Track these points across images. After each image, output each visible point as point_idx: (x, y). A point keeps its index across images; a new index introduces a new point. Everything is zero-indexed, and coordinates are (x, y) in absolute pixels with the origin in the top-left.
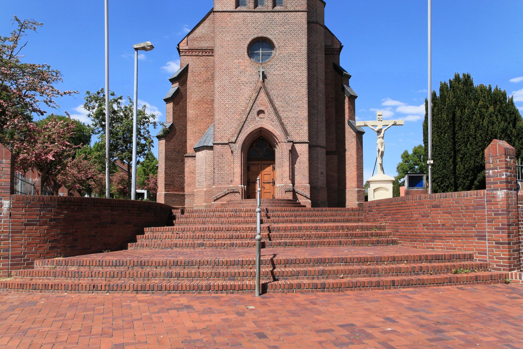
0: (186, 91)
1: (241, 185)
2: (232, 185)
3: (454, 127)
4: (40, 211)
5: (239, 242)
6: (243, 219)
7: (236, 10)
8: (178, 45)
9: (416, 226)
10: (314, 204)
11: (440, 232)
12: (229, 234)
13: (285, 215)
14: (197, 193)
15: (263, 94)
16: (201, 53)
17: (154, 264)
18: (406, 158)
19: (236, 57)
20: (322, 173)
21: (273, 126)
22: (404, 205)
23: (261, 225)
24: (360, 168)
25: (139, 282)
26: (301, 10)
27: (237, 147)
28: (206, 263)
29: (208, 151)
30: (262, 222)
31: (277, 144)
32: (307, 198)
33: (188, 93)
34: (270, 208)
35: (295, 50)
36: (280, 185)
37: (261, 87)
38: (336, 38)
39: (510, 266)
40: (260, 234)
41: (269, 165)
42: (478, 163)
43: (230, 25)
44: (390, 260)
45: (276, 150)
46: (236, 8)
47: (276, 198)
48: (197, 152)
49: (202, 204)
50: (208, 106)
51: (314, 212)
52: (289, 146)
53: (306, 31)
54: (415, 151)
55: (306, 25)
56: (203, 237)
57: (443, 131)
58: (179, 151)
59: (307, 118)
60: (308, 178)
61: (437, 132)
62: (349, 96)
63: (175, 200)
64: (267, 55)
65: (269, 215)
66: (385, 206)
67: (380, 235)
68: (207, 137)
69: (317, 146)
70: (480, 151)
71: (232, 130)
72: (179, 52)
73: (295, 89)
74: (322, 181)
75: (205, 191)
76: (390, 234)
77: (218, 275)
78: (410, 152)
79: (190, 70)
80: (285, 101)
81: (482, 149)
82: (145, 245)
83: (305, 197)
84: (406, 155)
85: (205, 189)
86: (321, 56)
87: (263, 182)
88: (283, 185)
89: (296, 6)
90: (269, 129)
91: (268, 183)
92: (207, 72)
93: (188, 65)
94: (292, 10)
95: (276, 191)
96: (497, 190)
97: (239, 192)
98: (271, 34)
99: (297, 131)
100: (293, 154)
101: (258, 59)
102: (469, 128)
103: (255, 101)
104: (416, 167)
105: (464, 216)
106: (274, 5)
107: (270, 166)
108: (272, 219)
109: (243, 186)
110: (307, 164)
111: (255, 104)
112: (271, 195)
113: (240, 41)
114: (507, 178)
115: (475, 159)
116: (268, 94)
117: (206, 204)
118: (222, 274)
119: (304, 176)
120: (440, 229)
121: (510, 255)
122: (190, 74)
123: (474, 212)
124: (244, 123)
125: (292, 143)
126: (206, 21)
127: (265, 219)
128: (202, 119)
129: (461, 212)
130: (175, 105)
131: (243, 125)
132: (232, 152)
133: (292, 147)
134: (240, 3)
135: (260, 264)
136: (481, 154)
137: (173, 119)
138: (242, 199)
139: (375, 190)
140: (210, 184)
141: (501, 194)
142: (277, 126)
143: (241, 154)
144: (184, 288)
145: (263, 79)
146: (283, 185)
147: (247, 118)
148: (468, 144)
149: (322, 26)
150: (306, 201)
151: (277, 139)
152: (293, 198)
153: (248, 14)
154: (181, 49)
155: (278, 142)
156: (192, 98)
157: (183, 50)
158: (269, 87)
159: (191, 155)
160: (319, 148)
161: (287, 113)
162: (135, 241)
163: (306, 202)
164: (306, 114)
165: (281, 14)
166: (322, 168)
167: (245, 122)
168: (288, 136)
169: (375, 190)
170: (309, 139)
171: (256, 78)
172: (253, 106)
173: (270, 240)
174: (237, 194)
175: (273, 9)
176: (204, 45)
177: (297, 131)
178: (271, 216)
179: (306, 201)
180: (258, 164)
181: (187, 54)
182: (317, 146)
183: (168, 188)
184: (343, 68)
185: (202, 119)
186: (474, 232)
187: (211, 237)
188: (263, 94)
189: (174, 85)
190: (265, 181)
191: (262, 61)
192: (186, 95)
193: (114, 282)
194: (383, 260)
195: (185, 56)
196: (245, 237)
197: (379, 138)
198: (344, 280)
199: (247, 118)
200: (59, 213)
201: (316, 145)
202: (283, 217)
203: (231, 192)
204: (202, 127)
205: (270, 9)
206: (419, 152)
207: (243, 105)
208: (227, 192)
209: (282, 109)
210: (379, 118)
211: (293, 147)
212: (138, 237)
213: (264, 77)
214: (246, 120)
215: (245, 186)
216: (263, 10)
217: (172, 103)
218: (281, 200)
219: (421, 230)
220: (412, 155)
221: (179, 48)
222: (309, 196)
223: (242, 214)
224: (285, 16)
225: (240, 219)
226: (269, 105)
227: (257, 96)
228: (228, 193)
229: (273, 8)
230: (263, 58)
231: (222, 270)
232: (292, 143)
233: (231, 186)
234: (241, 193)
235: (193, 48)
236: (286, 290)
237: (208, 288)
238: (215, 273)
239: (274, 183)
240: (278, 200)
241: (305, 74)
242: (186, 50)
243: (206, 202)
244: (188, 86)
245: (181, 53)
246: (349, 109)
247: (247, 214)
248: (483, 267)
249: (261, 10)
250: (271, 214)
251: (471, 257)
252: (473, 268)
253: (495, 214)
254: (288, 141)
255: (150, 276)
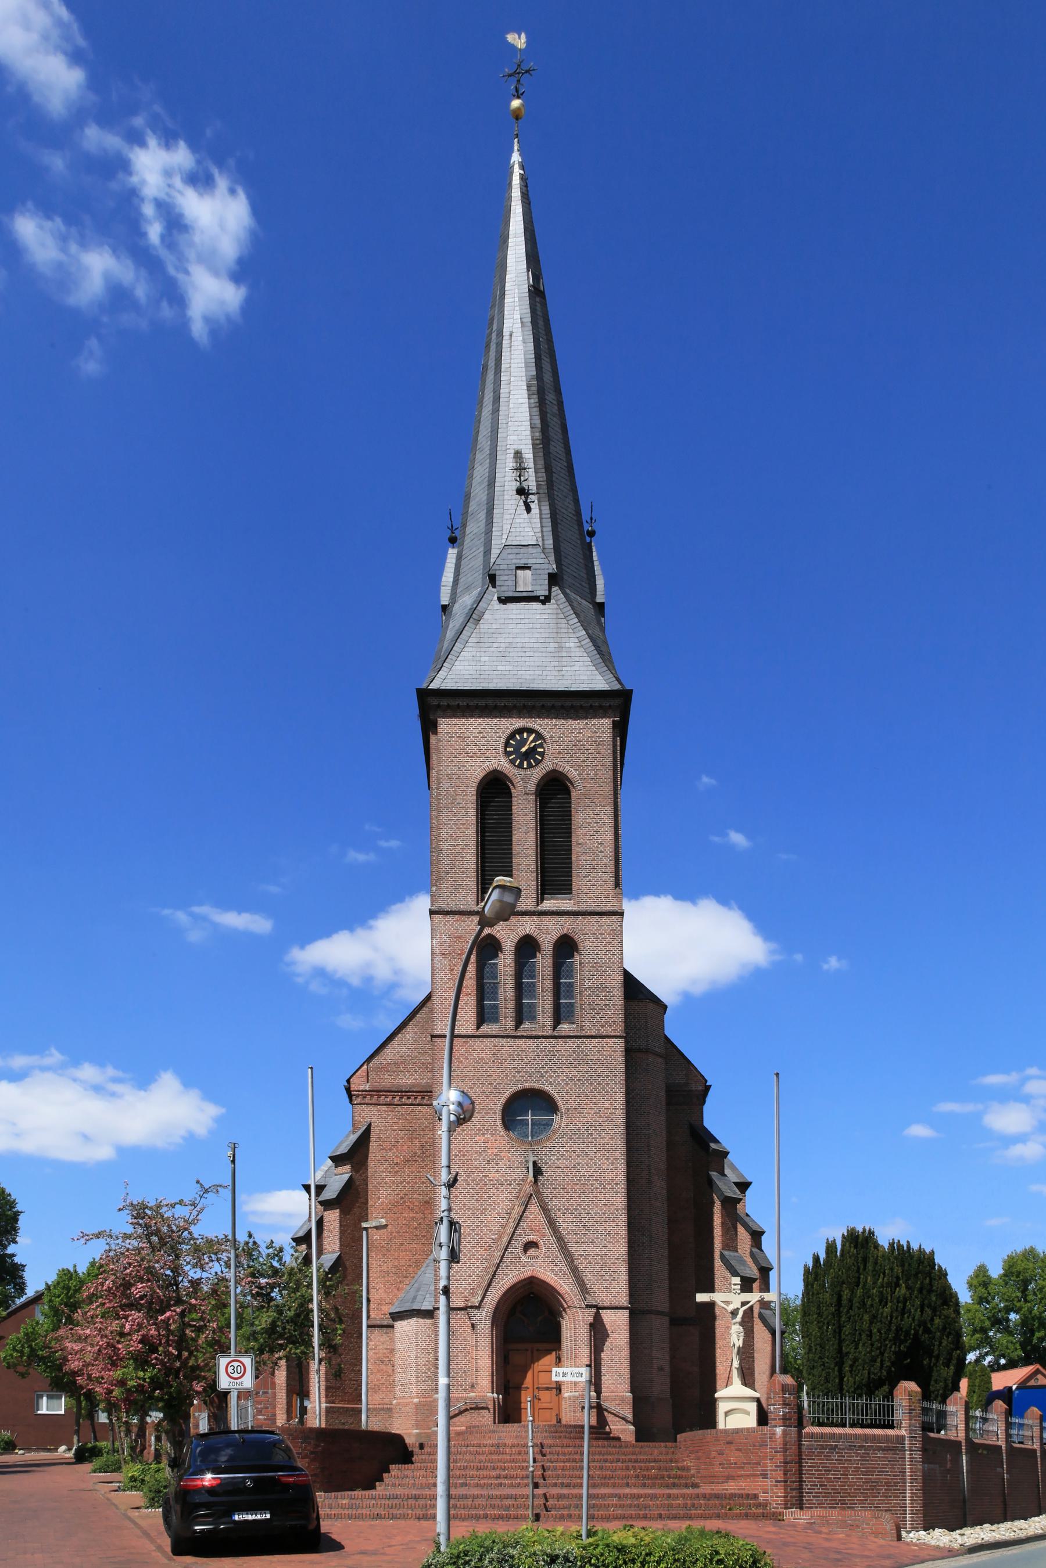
0: (365, 1181)
1: (493, 1393)
2: (474, 1394)
3: (840, 1317)
4: (302, 1443)
5: (506, 1481)
6: (508, 1457)
7: (477, 1033)
8: (348, 1081)
9: (713, 1465)
10: (643, 1434)
11: (732, 1472)
12: (494, 1473)
13: (566, 1452)
14: (398, 1407)
15: (534, 1209)
16: (398, 1098)
17: (428, 1497)
18: (982, 1290)
19: (479, 1130)
20: (661, 1369)
21: (556, 1274)
22: (704, 1441)
23: (535, 1490)
24: (747, 1357)
25: (419, 1512)
26: (613, 1034)
27: (484, 1317)
28: (480, 1497)
29: (421, 1320)
30: (535, 1461)
31: (564, 1310)
32: (627, 1422)
33: (370, 1187)
34: (545, 1442)
35: (600, 1117)
36: (572, 1394)
37: (531, 1195)
38: (696, 1069)
39: (785, 1504)
40: (533, 1467)
41: (548, 1352)
42: (874, 1374)
43: (465, 1063)
44: (665, 1496)
45: (563, 1323)
46: (478, 1027)
47: (564, 1422)
48: (397, 1321)
49: (409, 1431)
50: (414, 1215)
51: (610, 1449)
52: (589, 1316)
53: (623, 1078)
54: (1011, 1267)
55: (623, 1066)
56: (464, 1476)
57: (826, 1322)
58: (353, 1315)
59: (625, 1257)
60: (628, 1382)
61: (818, 1322)
62: (722, 1198)
63: (347, 1422)
64: (544, 1125)
65: (544, 1452)
66: (690, 1442)
67: (680, 1477)
68: (418, 1290)
69: (650, 1312)
70: (878, 1356)
71: (473, 1281)
72: (351, 1100)
73: (601, 1197)
74: (660, 1386)
75: (416, 1405)
76: (693, 1476)
77: (493, 1507)
78: (996, 1271)
79: (373, 1136)
80: (581, 1221)
81: (880, 1352)
82: (397, 1484)
83: (624, 1419)
84: (981, 1279)
85: (416, 1400)
86: (657, 1121)
87: (535, 1387)
88: (577, 1394)
89: (602, 1026)
90: (548, 1280)
91: (547, 1389)
92: (411, 1139)
93: (370, 1125)
94: (594, 1034)
95: (564, 1406)
96: (776, 1426)
97: (487, 1408)
98: (551, 1083)
99: (605, 1284)
100: (598, 1333)
101: (524, 1133)
102: (861, 1320)
103: (518, 1223)
104: (1013, 1316)
105: (752, 1453)
106: (557, 1022)
107: (551, 1353)
108: (548, 1457)
109: (495, 1395)
110: (625, 1352)
111: (519, 1229)
112: (554, 1414)
113: (487, 1097)
114: (783, 1415)
115: (870, 1369)
116: (545, 1209)
117: (417, 1431)
118: (497, 1505)
119: (620, 1376)
120: (732, 1468)
121: (785, 1493)
122: (373, 1146)
123: (759, 1449)
124: (497, 1268)
125: (594, 1310)
126: (409, 1028)
127: (539, 1457)
128: (402, 1244)
129: (750, 1450)
130: (344, 1214)
131: (495, 1272)
132: (473, 1326)
133: (594, 1318)
134: (486, 1016)
135: (533, 1498)
136: (879, 1360)
137: (341, 1245)
138: (495, 1423)
139: (727, 1414)
140: (425, 1390)
141: (779, 1430)
142: (565, 1273)
143: (492, 1331)
144: (463, 1517)
145: (535, 1176)
146: (577, 1394)
147: (502, 1257)
148: (861, 1345)
149: (657, 1055)
150: (625, 1427)
151: (565, 1301)
152: (597, 1423)
153: (503, 1041)
154: (354, 1091)
155: (566, 1306)
156: (379, 1198)
157: (359, 1091)
158: (546, 1191)
159: (379, 1323)
160: (653, 1316)
161: (584, 1247)
162: (381, 1480)
163: (623, 1429)
164: (621, 1248)
165: (570, 1041)
166: (661, 1357)
167: (499, 1265)
168: (588, 1293)
169: (727, 1414)
170: (631, 1295)
171: (519, 1173)
172: (514, 1232)
173: (544, 1480)
174: (484, 1412)
175: (554, 1030)
176: (406, 1080)
177: (605, 1284)
178: (548, 1452)
179: (625, 1427)
180: (527, 1350)
181: (367, 1100)
182: (650, 1312)
183: (332, 1396)
184: (712, 1133)
185: (402, 1244)
186: (758, 1471)
187: (475, 1476)
188: (534, 1209)
189: (340, 1170)
190: (540, 1386)
191: (532, 1138)
192: (367, 1191)
193: (394, 1511)
194: (658, 1496)
195: (364, 1104)
196: (515, 1476)
197: (734, 1324)
198: (469, 1395)
199: (502, 1257)
200: (317, 1446)
201: (647, 1310)
202: (565, 1454)
203: (472, 1409)
204: (403, 1262)
205: (548, 1031)
206: (1020, 1272)
207: (496, 1228)
208: (464, 1408)
209: (575, 1238)
210: (734, 1289)
211: (598, 1318)
212: (385, 1475)
213: (538, 1171)
214: (501, 1261)
215: (501, 1396)
216: (534, 1033)
217: (338, 1210)
218: (570, 1426)
219: (718, 1469)
220: (1001, 1277)
221: (350, 1088)
222: (630, 1417)
223: (507, 1450)
224: (578, 1046)
225: (505, 1457)
226: (548, 1232)
227: (524, 1212)
228: (466, 1410)
229: (555, 1028)
230: (534, 1130)
231: (497, 1502)
232: (594, 1310)
233: (472, 1394)
234: (492, 1410)
235: (380, 1088)
236: (557, 1520)
237: (486, 1516)
238: (491, 1505)
239: (560, 1390)
240: (565, 1426)
241: (621, 1167)
242: (366, 1091)
243: (417, 1427)
244: (369, 1170)
245: (354, 1098)
246: (722, 1226)
247: (514, 1450)
248: (765, 1505)
249: (529, 1033)
250: (548, 1450)
251: (756, 1496)
252: (750, 1506)
253: (775, 1452)
254: (587, 1306)
255: (428, 1507)
